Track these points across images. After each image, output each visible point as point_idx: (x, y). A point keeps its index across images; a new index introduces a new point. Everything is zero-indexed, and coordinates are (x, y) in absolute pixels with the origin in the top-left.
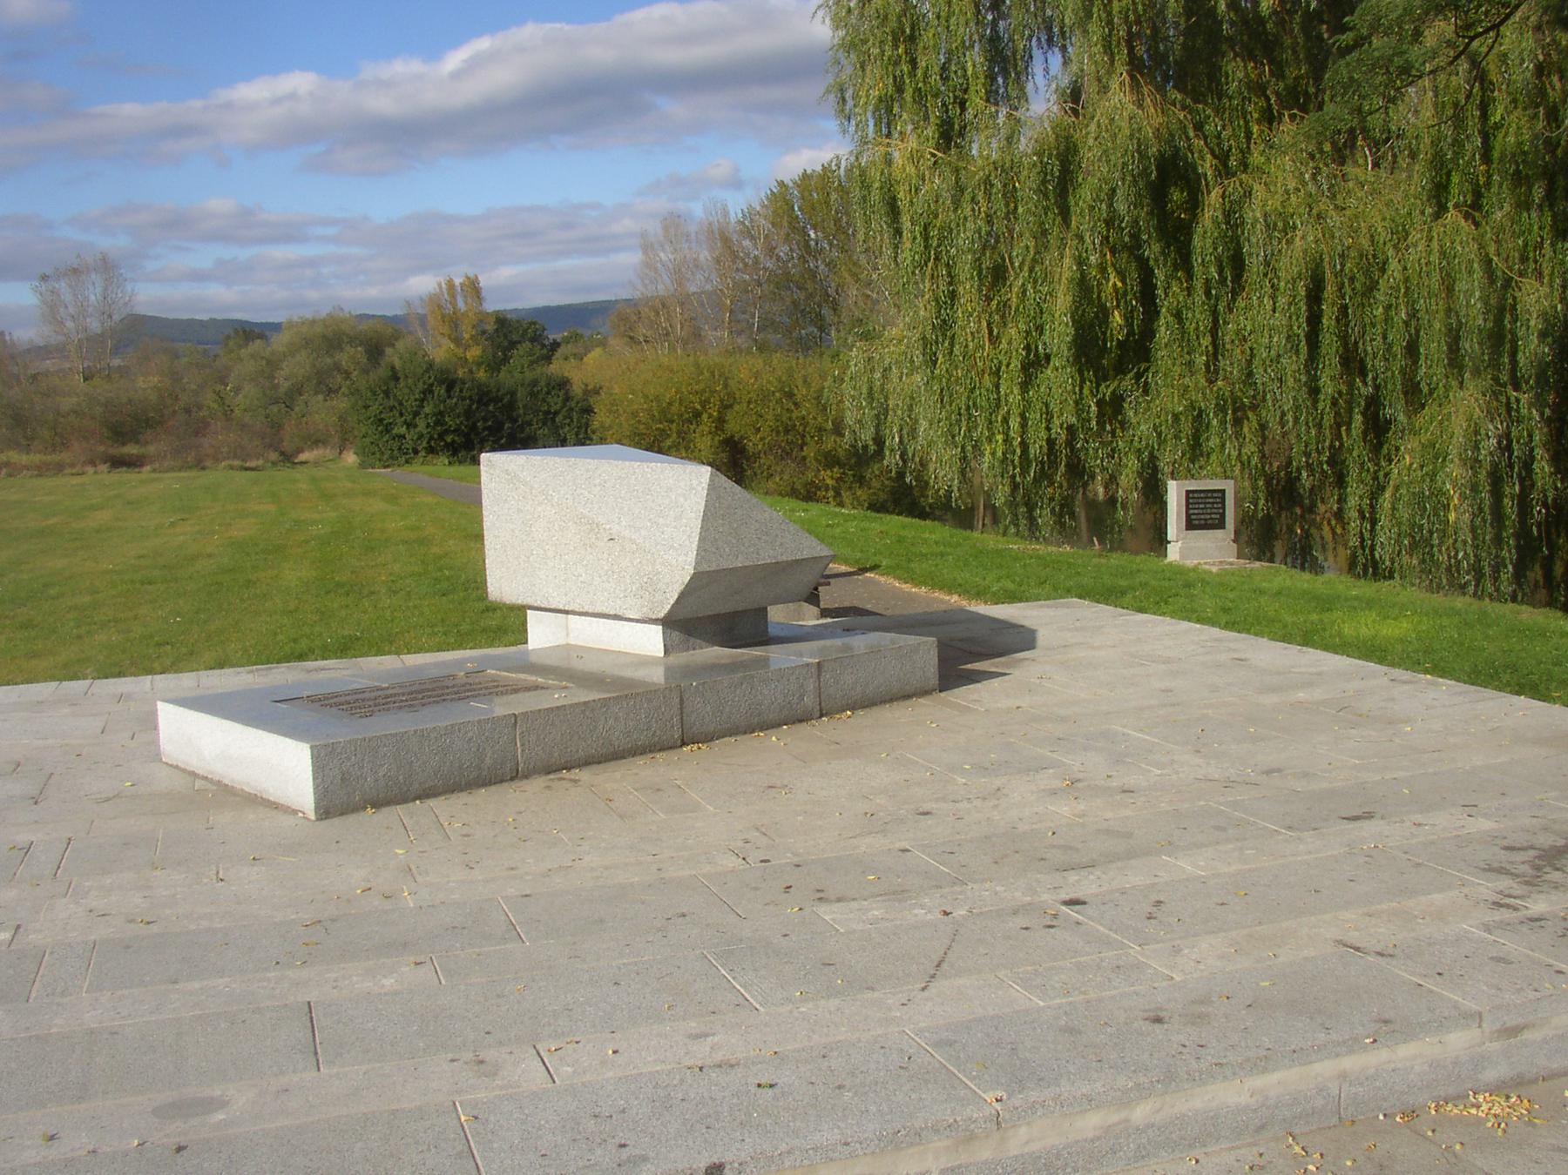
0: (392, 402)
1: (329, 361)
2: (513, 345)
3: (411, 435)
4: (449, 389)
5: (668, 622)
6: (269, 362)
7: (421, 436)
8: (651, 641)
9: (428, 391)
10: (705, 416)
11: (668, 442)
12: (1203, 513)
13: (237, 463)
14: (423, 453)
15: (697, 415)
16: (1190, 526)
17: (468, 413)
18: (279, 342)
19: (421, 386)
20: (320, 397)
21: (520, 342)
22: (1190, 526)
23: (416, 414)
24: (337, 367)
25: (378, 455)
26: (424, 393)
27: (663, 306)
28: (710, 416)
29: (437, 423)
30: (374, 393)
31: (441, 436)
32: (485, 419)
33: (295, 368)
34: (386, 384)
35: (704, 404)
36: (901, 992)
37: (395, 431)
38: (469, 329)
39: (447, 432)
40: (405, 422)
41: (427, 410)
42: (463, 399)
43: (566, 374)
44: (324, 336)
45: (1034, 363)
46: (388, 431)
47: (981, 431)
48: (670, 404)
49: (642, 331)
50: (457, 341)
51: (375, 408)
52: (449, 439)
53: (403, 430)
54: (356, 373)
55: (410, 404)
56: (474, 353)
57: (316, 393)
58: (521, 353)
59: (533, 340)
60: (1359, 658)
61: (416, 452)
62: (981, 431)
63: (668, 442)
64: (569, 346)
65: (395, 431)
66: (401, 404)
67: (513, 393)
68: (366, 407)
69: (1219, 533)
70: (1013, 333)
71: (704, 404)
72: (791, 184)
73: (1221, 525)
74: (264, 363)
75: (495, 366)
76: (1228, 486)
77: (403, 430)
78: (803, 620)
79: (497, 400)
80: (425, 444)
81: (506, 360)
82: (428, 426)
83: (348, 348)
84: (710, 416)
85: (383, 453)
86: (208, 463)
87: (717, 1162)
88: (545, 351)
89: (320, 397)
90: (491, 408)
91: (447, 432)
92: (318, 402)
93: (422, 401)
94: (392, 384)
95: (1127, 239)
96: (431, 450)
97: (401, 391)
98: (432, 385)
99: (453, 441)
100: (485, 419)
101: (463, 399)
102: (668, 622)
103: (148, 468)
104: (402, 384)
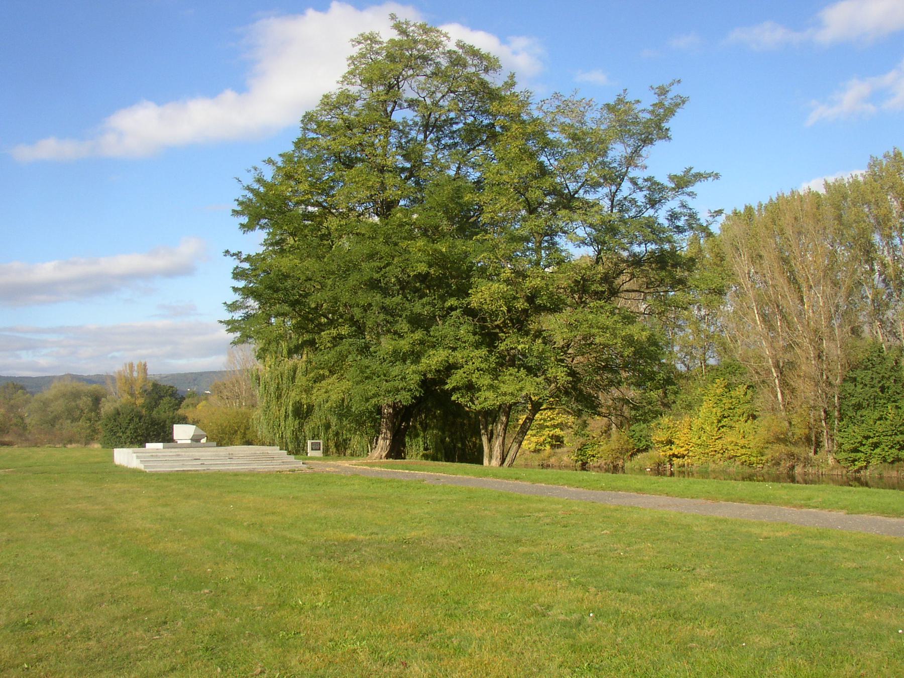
1: (73, 404)
2: (161, 397)
3: (124, 437)
4: (140, 418)
5: (191, 439)
6: (44, 404)
7: (128, 437)
8: (189, 442)
9: (131, 420)
10: (239, 432)
11: (225, 442)
12: (315, 447)
13: (52, 445)
14: (128, 444)
15: (236, 432)
16: (312, 449)
17: (147, 429)
18: (48, 394)
19: (129, 418)
20: (69, 421)
21: (164, 397)
22: (312, 449)
23: (126, 428)
24: (77, 407)
25: (110, 444)
26: (130, 420)
27: (237, 381)
28: (241, 432)
29: (135, 432)
31: (136, 437)
32: (154, 432)
33: (58, 406)
34: (115, 416)
35: (239, 427)
38: (139, 389)
41: (131, 427)
42: (146, 423)
43: (187, 415)
44: (72, 393)
45: (286, 417)
46: (115, 435)
47: (276, 430)
48: (226, 427)
49: (226, 393)
50: (132, 395)
51: (110, 426)
52: (139, 438)
53: (121, 434)
54: (87, 410)
55: (124, 425)
56: (140, 401)
57: (67, 419)
58: (165, 402)
59: (171, 395)
62: (276, 430)
63: (225, 442)
64: (190, 399)
67: (165, 421)
68: (106, 425)
69: (319, 451)
70: (283, 409)
71: (239, 427)
73: (319, 449)
74: (42, 404)
75: (151, 407)
76: (321, 441)
77: (121, 434)
79: (157, 424)
81: (157, 405)
82: (131, 433)
83: (84, 398)
84: (241, 432)
85: (112, 443)
86: (39, 445)
88: (177, 402)
89: (69, 421)
90: (156, 427)
91: (138, 436)
92: (68, 423)
93: (129, 423)
94: (117, 416)
97: (120, 419)
98: (133, 417)
99: (141, 440)
100: (154, 432)
101: (146, 423)
102: (191, 439)
103: (16, 446)
104: (121, 416)
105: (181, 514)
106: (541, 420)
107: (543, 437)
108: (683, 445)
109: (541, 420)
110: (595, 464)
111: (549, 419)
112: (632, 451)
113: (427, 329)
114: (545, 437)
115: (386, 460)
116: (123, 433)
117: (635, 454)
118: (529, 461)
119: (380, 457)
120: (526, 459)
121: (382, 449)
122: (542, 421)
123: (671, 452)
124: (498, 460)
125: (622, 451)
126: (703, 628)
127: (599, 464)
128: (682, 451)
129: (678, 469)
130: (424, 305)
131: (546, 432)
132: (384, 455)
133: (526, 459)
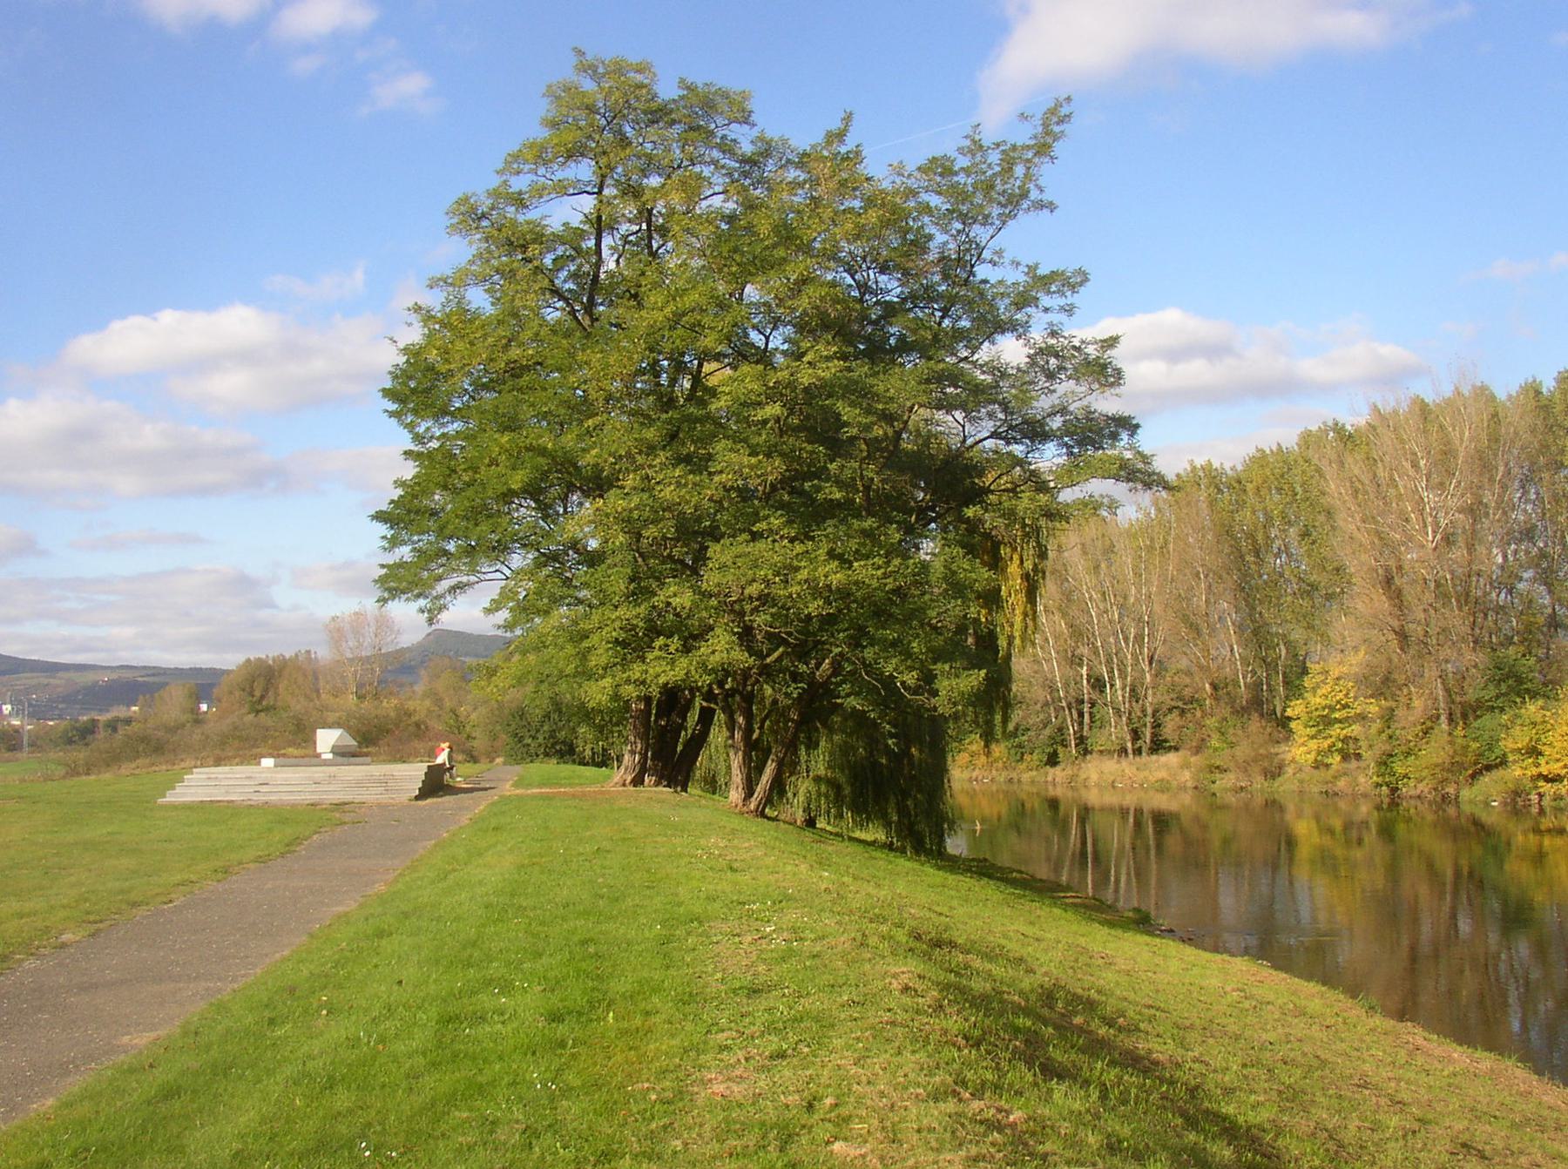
0: (524, 723)
7: (540, 745)
14: (542, 756)
23: (538, 731)
30: (514, 717)
36: (42, 896)
37: (525, 742)
39: (556, 743)
40: (530, 736)
41: (546, 728)
46: (520, 742)
52: (558, 748)
60: (390, 762)
61: (537, 756)
65: (525, 742)
66: (529, 724)
72: (1268, 452)
77: (529, 741)
78: (1093, 869)
80: (542, 750)
82: (545, 738)
87: (1397, 838)
91: (556, 743)
95: (1244, 703)
96: (547, 755)
99: (561, 749)
105: (767, 887)
106: (1324, 708)
107: (1329, 741)
108: (1559, 756)
109: (1324, 708)
110: (1412, 792)
111: (1338, 707)
112: (1474, 768)
113: (999, 543)
114: (1333, 740)
115: (632, 788)
116: (534, 738)
117: (1480, 772)
118: (1306, 785)
119: (621, 782)
120: (1301, 781)
121: (626, 770)
122: (1327, 710)
123: (1535, 771)
124: (740, 789)
125: (1454, 767)
126: (822, 1075)
127: (1418, 792)
128: (1556, 768)
129: (1553, 804)
130: (600, 521)
131: (1336, 730)
132: (629, 779)
133: (1301, 781)
